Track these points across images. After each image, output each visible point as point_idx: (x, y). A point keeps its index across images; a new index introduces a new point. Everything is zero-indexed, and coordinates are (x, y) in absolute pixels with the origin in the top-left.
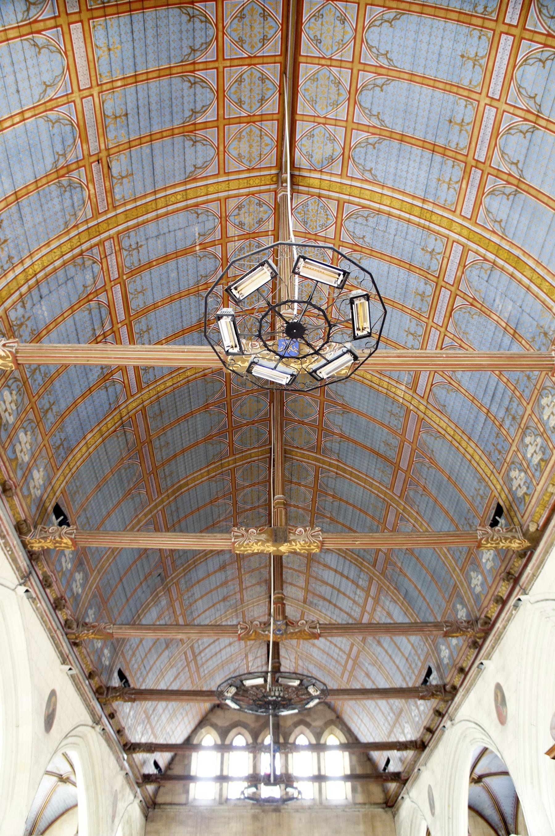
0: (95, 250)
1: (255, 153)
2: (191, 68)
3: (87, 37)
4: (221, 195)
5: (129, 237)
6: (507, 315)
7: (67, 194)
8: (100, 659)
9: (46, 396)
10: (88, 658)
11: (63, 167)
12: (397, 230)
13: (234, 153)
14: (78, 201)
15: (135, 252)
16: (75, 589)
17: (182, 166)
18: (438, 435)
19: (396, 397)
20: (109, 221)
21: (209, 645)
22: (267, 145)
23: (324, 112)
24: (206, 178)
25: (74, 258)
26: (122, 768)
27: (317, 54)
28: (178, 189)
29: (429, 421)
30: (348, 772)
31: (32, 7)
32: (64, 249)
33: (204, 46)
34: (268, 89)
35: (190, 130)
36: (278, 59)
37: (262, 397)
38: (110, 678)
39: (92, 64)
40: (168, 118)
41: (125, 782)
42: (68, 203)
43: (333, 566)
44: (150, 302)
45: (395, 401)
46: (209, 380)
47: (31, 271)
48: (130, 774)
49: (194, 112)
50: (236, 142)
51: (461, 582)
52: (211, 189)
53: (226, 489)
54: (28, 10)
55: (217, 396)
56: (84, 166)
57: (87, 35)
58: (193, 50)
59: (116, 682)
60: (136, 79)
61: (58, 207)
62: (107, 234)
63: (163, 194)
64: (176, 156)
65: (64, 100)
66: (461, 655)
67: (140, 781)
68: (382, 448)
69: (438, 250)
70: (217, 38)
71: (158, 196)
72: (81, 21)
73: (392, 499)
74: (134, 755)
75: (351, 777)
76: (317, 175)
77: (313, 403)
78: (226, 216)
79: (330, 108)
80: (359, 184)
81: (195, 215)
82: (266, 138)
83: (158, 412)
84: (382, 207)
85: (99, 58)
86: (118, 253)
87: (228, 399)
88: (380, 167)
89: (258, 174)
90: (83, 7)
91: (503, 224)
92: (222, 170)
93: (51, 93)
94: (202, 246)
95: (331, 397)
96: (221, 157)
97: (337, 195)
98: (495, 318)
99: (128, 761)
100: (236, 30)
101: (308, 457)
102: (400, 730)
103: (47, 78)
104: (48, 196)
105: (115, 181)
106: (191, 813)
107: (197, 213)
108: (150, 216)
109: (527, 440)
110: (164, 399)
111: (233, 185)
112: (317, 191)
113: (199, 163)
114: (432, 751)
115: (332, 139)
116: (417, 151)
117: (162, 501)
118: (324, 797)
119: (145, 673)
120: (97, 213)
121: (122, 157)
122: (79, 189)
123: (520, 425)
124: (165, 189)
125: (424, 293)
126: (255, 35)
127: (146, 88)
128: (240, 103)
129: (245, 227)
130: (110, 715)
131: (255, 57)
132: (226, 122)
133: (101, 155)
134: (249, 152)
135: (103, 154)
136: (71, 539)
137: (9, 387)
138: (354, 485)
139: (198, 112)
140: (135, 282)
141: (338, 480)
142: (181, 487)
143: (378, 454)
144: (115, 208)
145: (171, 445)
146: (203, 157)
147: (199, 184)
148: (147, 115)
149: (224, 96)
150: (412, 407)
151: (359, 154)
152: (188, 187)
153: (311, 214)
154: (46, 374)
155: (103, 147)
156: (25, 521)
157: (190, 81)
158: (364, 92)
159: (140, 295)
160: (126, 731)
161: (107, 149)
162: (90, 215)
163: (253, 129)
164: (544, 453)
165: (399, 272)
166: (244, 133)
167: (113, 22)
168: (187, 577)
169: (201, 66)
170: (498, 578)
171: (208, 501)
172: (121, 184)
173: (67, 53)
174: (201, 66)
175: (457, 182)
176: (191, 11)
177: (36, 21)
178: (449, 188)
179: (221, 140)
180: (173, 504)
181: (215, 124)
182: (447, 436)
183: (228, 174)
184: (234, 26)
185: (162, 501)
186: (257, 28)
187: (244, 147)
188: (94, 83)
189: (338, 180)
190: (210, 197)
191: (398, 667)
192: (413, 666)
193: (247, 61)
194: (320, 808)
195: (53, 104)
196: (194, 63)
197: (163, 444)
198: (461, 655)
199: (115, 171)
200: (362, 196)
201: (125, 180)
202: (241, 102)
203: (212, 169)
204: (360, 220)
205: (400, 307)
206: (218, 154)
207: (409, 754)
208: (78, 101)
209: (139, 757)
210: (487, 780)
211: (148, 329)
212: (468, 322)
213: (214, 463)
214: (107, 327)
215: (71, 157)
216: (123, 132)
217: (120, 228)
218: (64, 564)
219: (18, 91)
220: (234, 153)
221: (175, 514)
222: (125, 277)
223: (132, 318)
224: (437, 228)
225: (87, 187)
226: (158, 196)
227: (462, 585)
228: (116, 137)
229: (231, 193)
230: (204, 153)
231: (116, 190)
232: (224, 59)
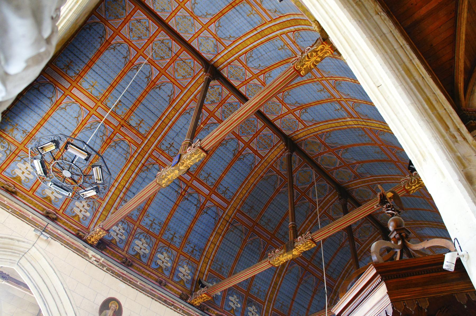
0: (150, 160)
1: (189, 70)
2: (131, 64)
3: (81, 89)
4: (191, 98)
5: (163, 144)
11: (107, 140)
13: (180, 77)
14: (125, 146)
15: (172, 148)
17: (163, 100)
20: (148, 144)
22: (190, 63)
23: (193, 31)
24: (178, 96)
27: (168, 15)
28: (170, 110)
31: (52, 99)
32: (132, 168)
33: (128, 53)
34: (168, 43)
35: (153, 85)
36: (159, 30)
39: (90, 96)
40: (139, 88)
42: (120, 150)
47: (120, 187)
49: (148, 77)
50: (176, 73)
52: (185, 99)
54: (52, 100)
55: (279, 183)
56: (117, 132)
57: (80, 89)
58: (126, 58)
60: (113, 87)
61: (117, 155)
62: (151, 150)
63: (164, 117)
64: (156, 98)
65: (89, 116)
70: (130, 46)
71: (163, 119)
72: (74, 87)
76: (219, 57)
77: (331, 156)
79: (193, 28)
81: (187, 114)
82: (186, 61)
83: (249, 208)
85: (91, 93)
86: (163, 154)
88: (231, 31)
89: (199, 77)
90: (72, 82)
92: (182, 88)
93: (81, 119)
94: (204, 124)
95: (334, 147)
96: (176, 83)
100: (134, 36)
101: (359, 183)
103: (75, 115)
104: (108, 154)
105: (137, 128)
107: (187, 113)
111: (193, 90)
112: (226, 63)
113: (169, 93)
115: (208, 38)
116: (230, 13)
120: (138, 146)
121: (132, 117)
122: (122, 142)
124: (164, 114)
126: (143, 31)
127: (120, 86)
128: (162, 58)
129: (216, 101)
131: (150, 37)
132: (164, 69)
133: (121, 123)
135: (122, 122)
136: (205, 293)
137: (138, 238)
139: (150, 76)
143: (381, 161)
146: (168, 90)
147: (177, 101)
148: (129, 94)
149: (154, 61)
151: (220, 34)
152: (173, 106)
153: (235, 73)
154: (160, 224)
155: (120, 120)
156: (182, 293)
157: (135, 69)
158: (194, 11)
161: (123, 119)
162: (135, 148)
163: (178, 62)
166: (176, 67)
167: (87, 77)
169: (134, 60)
172: (141, 127)
173: (77, 100)
174: (134, 60)
175: (252, 10)
176: (112, 47)
177: (57, 101)
179: (170, 77)
181: (161, 74)
183: (186, 87)
184: (132, 36)
186: (141, 28)
187: (182, 72)
188: (96, 102)
190: (187, 102)
193: (149, 42)
195: (85, 121)
196: (130, 61)
199: (133, 124)
201: (141, 125)
202: (162, 57)
203: (177, 91)
206: (174, 84)
208: (95, 113)
211: (209, 175)
213: (310, 215)
214: (184, 186)
215: (108, 134)
216: (124, 107)
217: (155, 143)
218: (233, 306)
219: (66, 128)
220: (180, 77)
223: (195, 175)
225: (125, 139)
228: (122, 112)
229: (195, 93)
230: (168, 89)
232: (140, 50)
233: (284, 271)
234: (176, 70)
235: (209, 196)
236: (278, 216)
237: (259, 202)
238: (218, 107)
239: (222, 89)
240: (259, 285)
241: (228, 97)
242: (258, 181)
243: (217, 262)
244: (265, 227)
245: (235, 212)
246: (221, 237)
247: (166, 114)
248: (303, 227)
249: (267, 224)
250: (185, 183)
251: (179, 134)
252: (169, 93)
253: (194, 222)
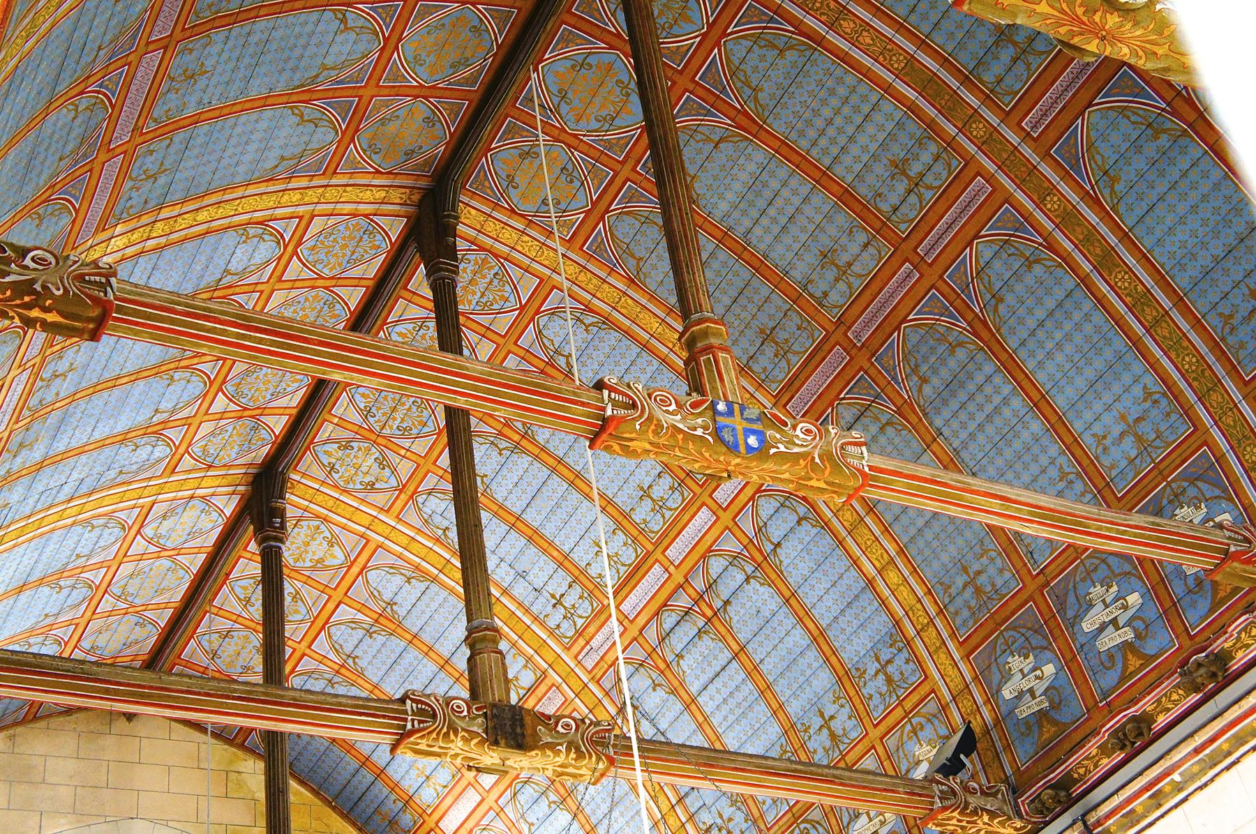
34: (245, 588)
44: (843, 218)
46: (632, 262)
78: (401, 491)
83: (769, 350)
87: (626, 172)
96: (362, 560)
134: (313, 539)
145: (825, 241)
181: (346, 600)
203: (381, 558)
223: (651, 547)
230: (386, 583)
233: (1093, 219)
234: (318, 562)
236: (808, 210)
237: (742, 300)
238: (396, 448)
239: (328, 441)
240: (1107, 418)
241: (342, 423)
242: (652, 298)
243: (953, 591)
244: (858, 285)
246: (868, 520)
248: (867, 61)
249: (843, 271)
250: (675, 591)
252: (399, 580)
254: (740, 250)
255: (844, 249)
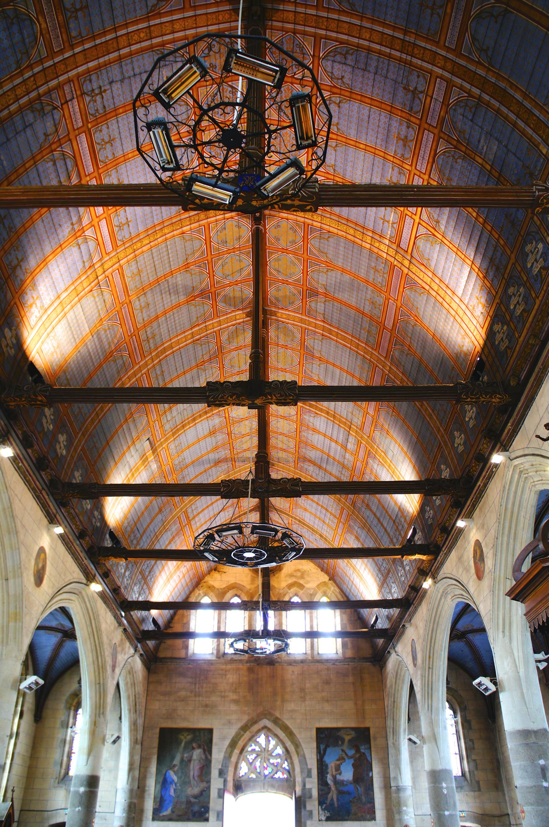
5: (90, 81)
6: (491, 157)
7: (15, 28)
8: (90, 520)
9: (12, 252)
10: (77, 519)
12: (377, 67)
16: (59, 451)
18: (423, 290)
19: (380, 253)
21: (203, 510)
24: (171, 13)
25: (31, 102)
26: (120, 624)
29: (413, 276)
30: (339, 628)
37: (243, 256)
38: (103, 539)
41: (124, 637)
42: (17, 38)
43: (322, 430)
45: (379, 257)
46: (187, 238)
48: (129, 630)
51: (445, 442)
53: (212, 352)
59: (108, 543)
62: (65, 77)
66: (444, 515)
67: (140, 637)
68: (367, 307)
69: (420, 88)
73: (378, 360)
74: (132, 613)
75: (342, 634)
77: (296, 262)
80: (335, 16)
83: (135, 271)
84: (361, 42)
86: (80, 99)
87: (209, 258)
91: (490, 53)
95: (315, 255)
97: (313, 30)
98: (480, 161)
99: (126, 617)
102: (388, 590)
105: (69, 14)
106: (190, 666)
108: (112, 56)
109: (511, 290)
110: (141, 258)
114: (416, 609)
117: (146, 364)
118: (316, 652)
119: (138, 535)
122: (27, 23)
123: (503, 275)
125: (406, 137)
130: (104, 574)
138: (341, 346)
140: (101, 131)
141: (324, 341)
142: (165, 350)
144: (72, 47)
145: (151, 306)
147: (164, 20)
150: (396, 263)
159: (108, 145)
160: (123, 590)
164: (526, 303)
165: (380, 115)
168: (177, 442)
170: (480, 436)
171: (194, 364)
172: (76, 18)
175: (441, 7)
178: (432, 14)
180: (158, 368)
182: (431, 291)
185: (146, 364)
189: (313, 12)
191: (386, 530)
192: (400, 528)
194: (314, 662)
197: (143, 304)
198: (444, 515)
200: (339, 30)
201: (80, 14)
204: (338, 58)
205: (382, 154)
207: (395, 612)
209: (137, 614)
210: (470, 636)
212: (452, 167)
213: (198, 325)
217: (80, 69)
218: (45, 425)
221: (160, 378)
222: (90, 126)
223: (101, 171)
224: (419, 62)
225: (38, 19)
226: (120, 33)
227: (446, 445)
231: (72, 26)
235: (97, 220)
236: (161, 305)
245: (114, 267)
247: (130, 29)
248: (179, 337)
251: (126, 81)
252: (165, 217)
253: (56, 253)
254: (170, 543)
255: (146, 312)
